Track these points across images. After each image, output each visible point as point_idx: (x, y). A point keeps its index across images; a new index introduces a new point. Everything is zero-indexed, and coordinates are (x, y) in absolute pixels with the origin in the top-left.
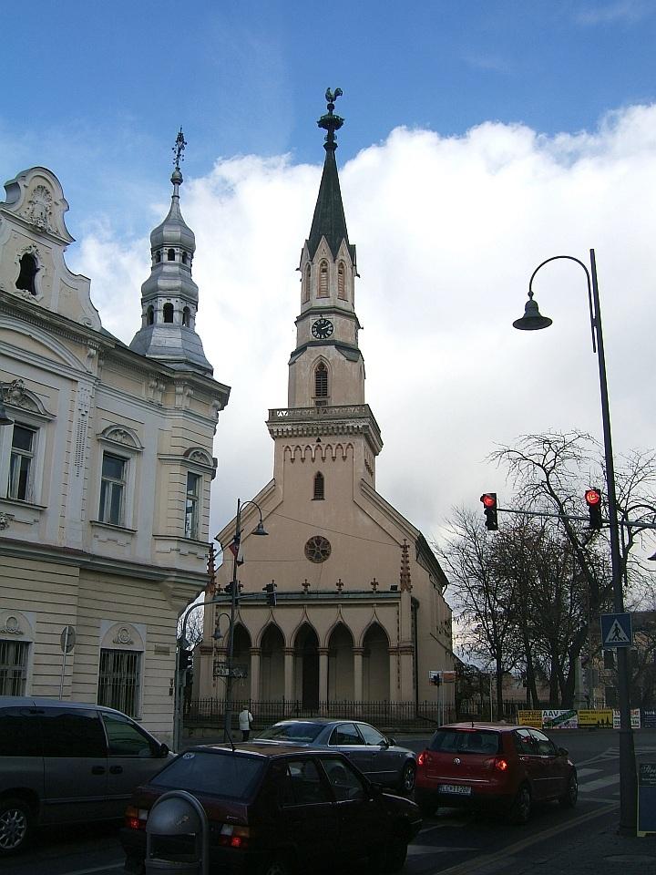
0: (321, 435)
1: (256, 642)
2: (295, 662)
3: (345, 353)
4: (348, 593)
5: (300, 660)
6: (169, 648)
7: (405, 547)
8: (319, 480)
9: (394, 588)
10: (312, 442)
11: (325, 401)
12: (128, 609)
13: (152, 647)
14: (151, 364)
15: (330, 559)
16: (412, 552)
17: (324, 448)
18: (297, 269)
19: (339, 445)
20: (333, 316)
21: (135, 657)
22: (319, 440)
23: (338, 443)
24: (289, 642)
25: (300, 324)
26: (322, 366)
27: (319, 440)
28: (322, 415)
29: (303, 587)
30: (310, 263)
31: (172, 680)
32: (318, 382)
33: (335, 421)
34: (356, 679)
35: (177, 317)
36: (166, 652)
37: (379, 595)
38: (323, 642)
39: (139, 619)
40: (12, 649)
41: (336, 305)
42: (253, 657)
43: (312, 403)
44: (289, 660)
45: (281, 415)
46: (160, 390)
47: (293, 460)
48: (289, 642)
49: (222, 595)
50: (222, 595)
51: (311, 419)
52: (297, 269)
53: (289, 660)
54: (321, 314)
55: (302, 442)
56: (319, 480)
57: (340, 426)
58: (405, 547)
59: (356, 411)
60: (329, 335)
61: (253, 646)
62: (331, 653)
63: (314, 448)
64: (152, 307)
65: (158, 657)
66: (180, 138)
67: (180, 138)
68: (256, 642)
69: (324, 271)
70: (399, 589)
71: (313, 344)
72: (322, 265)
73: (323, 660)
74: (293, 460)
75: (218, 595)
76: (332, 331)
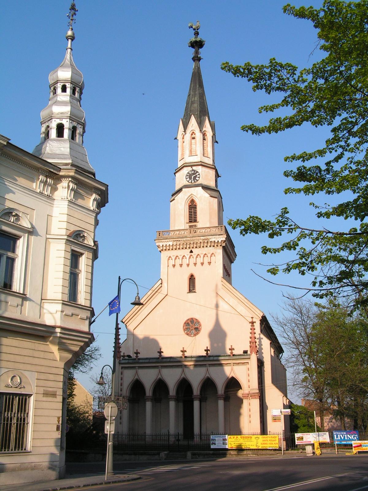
0: (193, 248)
1: (149, 391)
2: (177, 407)
3: (209, 192)
4: (213, 356)
5: (181, 405)
6: (56, 392)
7: (253, 323)
8: (192, 279)
9: (245, 352)
10: (187, 252)
11: (195, 225)
12: (18, 359)
13: (41, 390)
14: (42, 164)
15: (185, 320)
16: (257, 326)
17: (195, 257)
19: (205, 254)
20: (200, 167)
21: (26, 399)
22: (191, 252)
23: (204, 253)
24: (172, 391)
26: (193, 201)
27: (191, 252)
28: (193, 234)
29: (182, 353)
30: (184, 133)
31: (59, 418)
32: (190, 213)
33: (202, 238)
34: (170, 413)
35: (66, 133)
36: (54, 395)
37: (235, 357)
38: (196, 390)
39: (29, 367)
40: (16, 400)
41: (202, 161)
42: (147, 403)
43: (187, 226)
44: (172, 404)
46: (50, 185)
47: (174, 266)
48: (172, 391)
49: (125, 359)
50: (125, 359)
51: (186, 237)
53: (172, 404)
54: (192, 166)
55: (180, 253)
56: (192, 279)
57: (206, 241)
58: (253, 323)
59: (217, 231)
60: (197, 180)
61: (147, 395)
62: (203, 399)
63: (188, 257)
64: (48, 127)
65: (45, 399)
66: (73, 8)
67: (73, 8)
68: (149, 391)
69: (194, 138)
70: (249, 352)
71: (186, 186)
72: (192, 135)
73: (196, 404)
74: (174, 266)
75: (123, 359)
76: (199, 177)
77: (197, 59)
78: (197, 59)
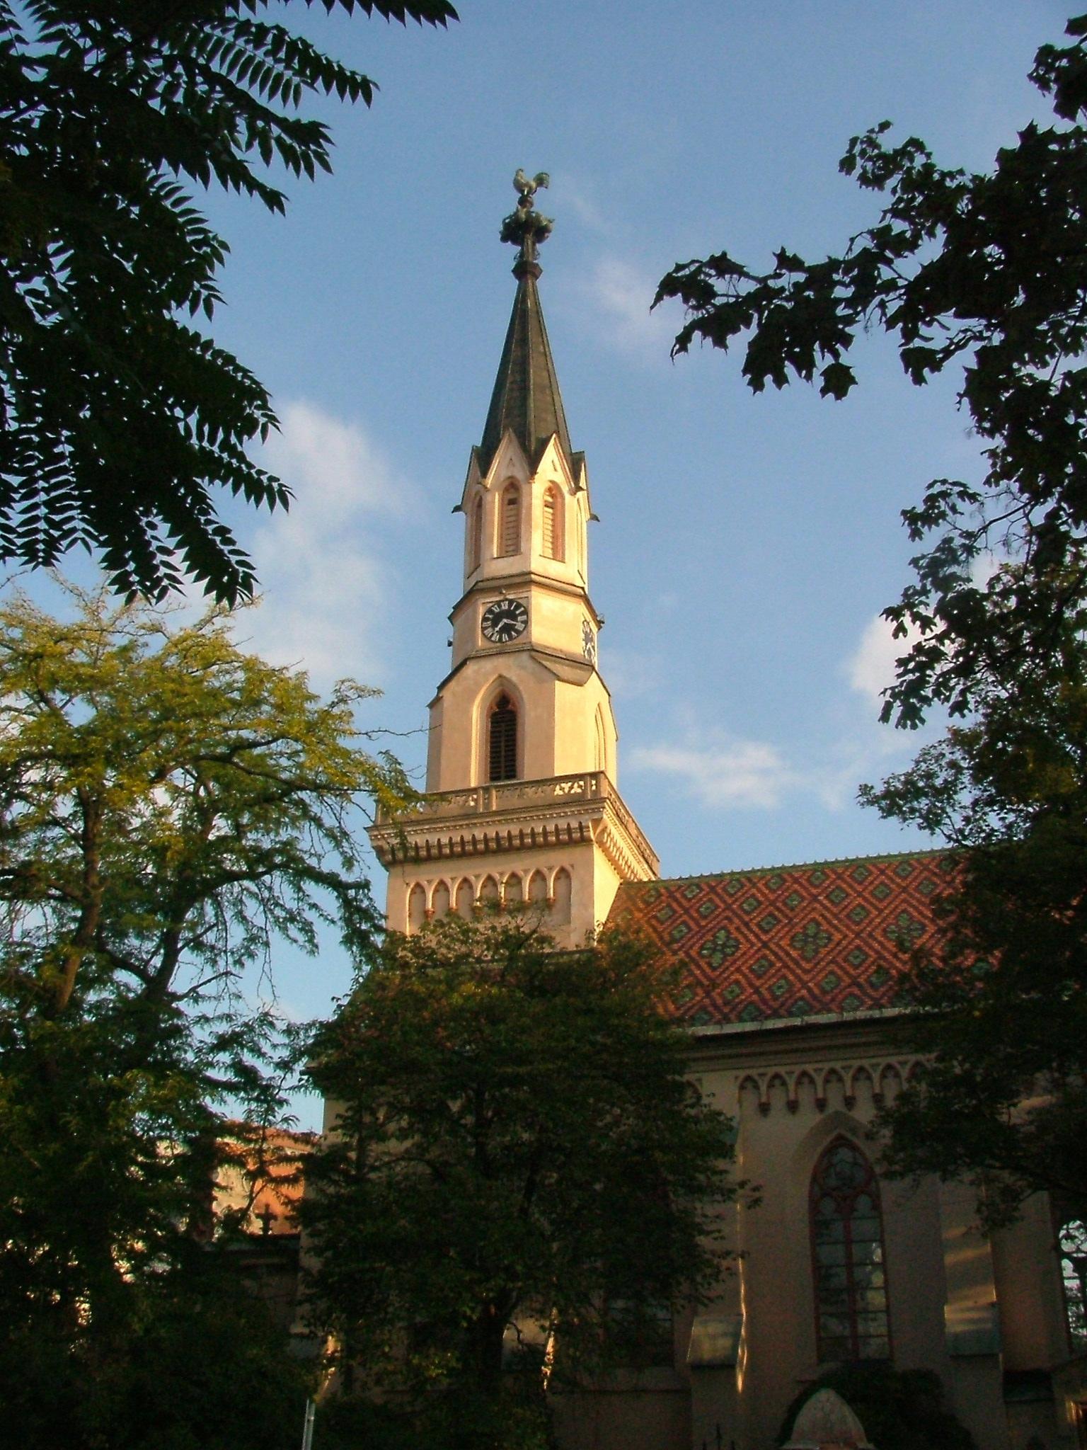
18: (457, 509)
25: (460, 620)
45: (558, 792)
52: (457, 509)
54: (497, 590)
77: (525, 270)
78: (525, 270)
